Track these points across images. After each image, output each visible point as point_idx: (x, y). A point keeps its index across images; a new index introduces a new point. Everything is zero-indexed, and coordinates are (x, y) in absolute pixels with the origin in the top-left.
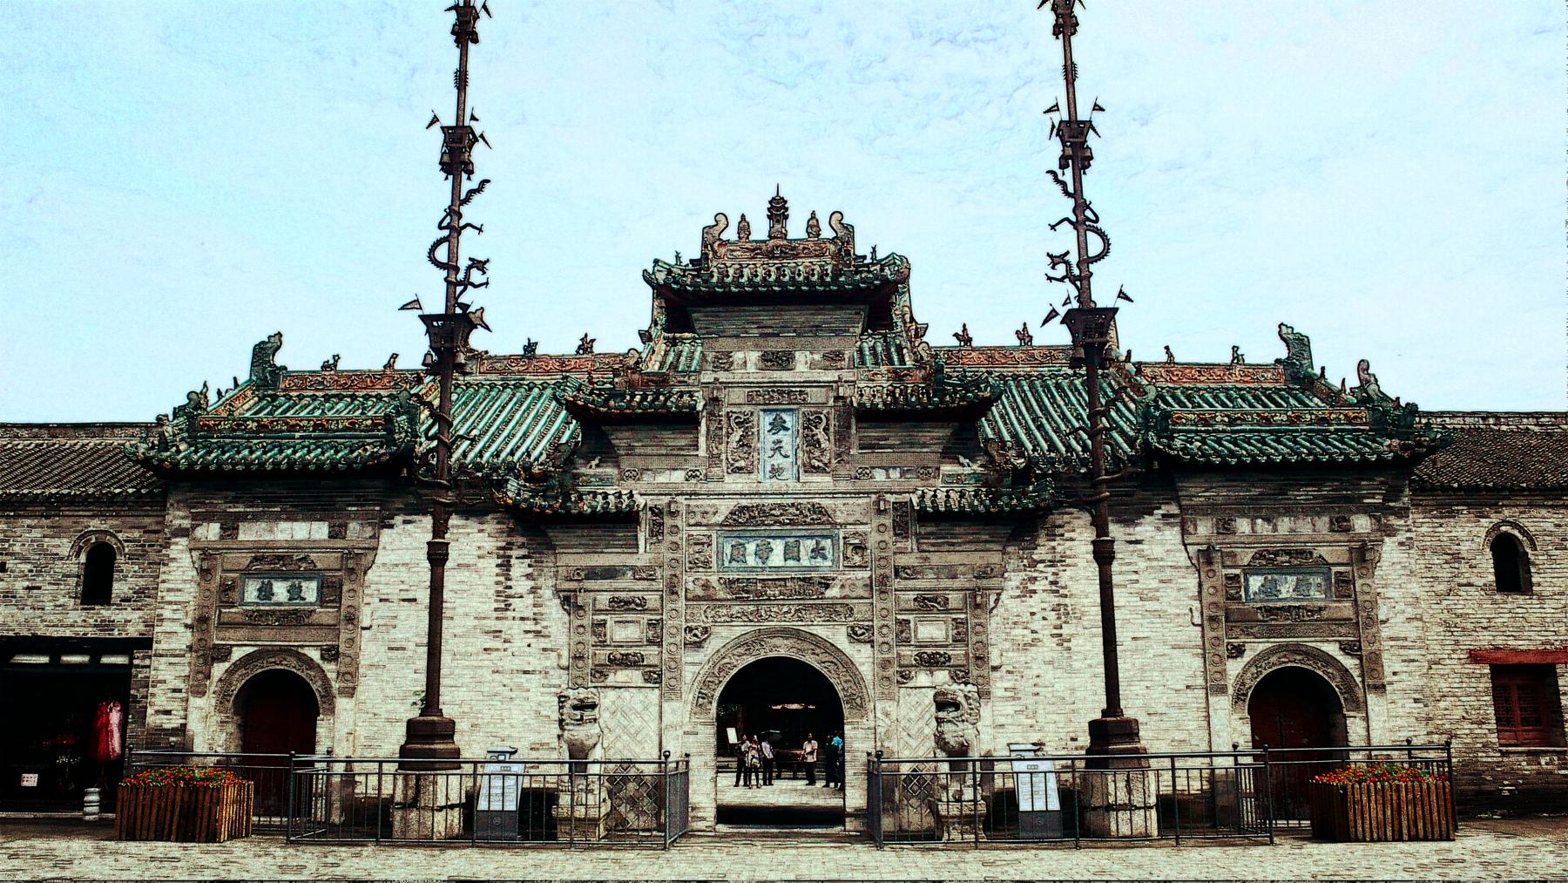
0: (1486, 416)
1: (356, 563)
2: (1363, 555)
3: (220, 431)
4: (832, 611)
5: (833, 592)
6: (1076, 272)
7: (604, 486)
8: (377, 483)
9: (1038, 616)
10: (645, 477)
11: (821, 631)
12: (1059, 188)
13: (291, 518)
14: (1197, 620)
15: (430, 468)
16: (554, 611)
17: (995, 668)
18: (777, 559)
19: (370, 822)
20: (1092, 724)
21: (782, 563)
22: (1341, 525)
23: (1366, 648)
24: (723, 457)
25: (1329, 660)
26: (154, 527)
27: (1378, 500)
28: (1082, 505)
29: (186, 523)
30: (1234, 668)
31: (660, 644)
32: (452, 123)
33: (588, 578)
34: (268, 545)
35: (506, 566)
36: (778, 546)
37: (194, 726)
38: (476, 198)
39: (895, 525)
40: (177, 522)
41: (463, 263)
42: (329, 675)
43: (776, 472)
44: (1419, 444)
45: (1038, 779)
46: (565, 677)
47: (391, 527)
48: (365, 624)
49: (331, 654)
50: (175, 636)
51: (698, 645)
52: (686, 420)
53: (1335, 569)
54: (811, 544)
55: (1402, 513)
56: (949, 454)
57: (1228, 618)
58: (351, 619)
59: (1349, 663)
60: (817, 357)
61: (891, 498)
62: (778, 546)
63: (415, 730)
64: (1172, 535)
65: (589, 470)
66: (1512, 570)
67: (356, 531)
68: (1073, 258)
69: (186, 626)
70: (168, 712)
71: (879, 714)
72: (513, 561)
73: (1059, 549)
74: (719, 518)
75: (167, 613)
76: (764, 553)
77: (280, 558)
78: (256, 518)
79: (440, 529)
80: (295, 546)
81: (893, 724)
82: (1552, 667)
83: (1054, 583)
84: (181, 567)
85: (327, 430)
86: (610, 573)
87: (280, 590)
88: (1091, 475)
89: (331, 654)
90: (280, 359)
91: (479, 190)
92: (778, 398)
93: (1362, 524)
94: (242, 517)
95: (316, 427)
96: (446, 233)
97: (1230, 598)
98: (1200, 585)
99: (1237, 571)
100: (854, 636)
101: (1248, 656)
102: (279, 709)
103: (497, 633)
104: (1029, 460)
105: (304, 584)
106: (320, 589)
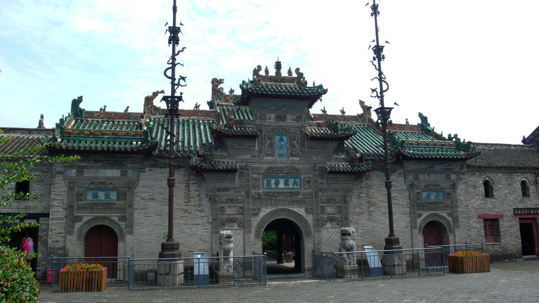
0: (486, 144)
1: (131, 186)
2: (454, 186)
3: (74, 134)
4: (300, 203)
5: (300, 197)
6: (379, 95)
7: (224, 160)
8: (140, 156)
9: (363, 205)
10: (237, 157)
11: (296, 210)
12: (374, 67)
13: (105, 168)
14: (409, 206)
15: (167, 152)
16: (206, 203)
17: (350, 221)
18: (281, 185)
19: (146, 280)
20: (386, 239)
21: (283, 187)
22: (448, 178)
23: (455, 214)
24: (263, 150)
25: (444, 218)
26: (47, 171)
27: (458, 170)
28: (382, 170)
29: (62, 169)
30: (419, 221)
31: (244, 214)
32: (172, 26)
33: (218, 191)
34: (97, 178)
35: (188, 186)
36: (282, 181)
37: (69, 246)
38: (181, 53)
39: (320, 175)
40: (57, 169)
41: (177, 77)
42: (122, 226)
43: (281, 155)
44: (472, 154)
45: (372, 257)
46: (210, 226)
47: (144, 172)
48: (136, 207)
49: (123, 219)
50: (58, 211)
51: (256, 215)
52: (253, 137)
53: (446, 190)
54: (293, 180)
55: (463, 174)
56: (336, 152)
57: (417, 205)
58: (131, 206)
59: (450, 219)
60: (294, 117)
61: (318, 165)
62: (282, 181)
63: (164, 247)
64: (401, 179)
65: (219, 153)
66: (489, 191)
67: (131, 173)
68: (379, 90)
69: (64, 209)
70: (57, 241)
71: (315, 237)
72: (190, 185)
73: (369, 183)
74: (262, 171)
75: (55, 203)
76: (277, 183)
77: (101, 183)
78: (91, 167)
79: (171, 174)
80: (109, 178)
81: (324, 239)
82: (498, 219)
83: (367, 194)
84: (60, 187)
85: (117, 135)
86: (226, 189)
87: (101, 196)
88: (384, 161)
89: (123, 219)
90: (82, 106)
91: (182, 51)
92: (282, 131)
93: (453, 177)
94: (85, 167)
95: (113, 134)
96: (171, 66)
97: (418, 199)
98: (410, 195)
99: (420, 191)
100: (307, 212)
101: (423, 217)
102: (102, 240)
103: (186, 211)
104: (361, 154)
105: (111, 193)
106: (118, 194)
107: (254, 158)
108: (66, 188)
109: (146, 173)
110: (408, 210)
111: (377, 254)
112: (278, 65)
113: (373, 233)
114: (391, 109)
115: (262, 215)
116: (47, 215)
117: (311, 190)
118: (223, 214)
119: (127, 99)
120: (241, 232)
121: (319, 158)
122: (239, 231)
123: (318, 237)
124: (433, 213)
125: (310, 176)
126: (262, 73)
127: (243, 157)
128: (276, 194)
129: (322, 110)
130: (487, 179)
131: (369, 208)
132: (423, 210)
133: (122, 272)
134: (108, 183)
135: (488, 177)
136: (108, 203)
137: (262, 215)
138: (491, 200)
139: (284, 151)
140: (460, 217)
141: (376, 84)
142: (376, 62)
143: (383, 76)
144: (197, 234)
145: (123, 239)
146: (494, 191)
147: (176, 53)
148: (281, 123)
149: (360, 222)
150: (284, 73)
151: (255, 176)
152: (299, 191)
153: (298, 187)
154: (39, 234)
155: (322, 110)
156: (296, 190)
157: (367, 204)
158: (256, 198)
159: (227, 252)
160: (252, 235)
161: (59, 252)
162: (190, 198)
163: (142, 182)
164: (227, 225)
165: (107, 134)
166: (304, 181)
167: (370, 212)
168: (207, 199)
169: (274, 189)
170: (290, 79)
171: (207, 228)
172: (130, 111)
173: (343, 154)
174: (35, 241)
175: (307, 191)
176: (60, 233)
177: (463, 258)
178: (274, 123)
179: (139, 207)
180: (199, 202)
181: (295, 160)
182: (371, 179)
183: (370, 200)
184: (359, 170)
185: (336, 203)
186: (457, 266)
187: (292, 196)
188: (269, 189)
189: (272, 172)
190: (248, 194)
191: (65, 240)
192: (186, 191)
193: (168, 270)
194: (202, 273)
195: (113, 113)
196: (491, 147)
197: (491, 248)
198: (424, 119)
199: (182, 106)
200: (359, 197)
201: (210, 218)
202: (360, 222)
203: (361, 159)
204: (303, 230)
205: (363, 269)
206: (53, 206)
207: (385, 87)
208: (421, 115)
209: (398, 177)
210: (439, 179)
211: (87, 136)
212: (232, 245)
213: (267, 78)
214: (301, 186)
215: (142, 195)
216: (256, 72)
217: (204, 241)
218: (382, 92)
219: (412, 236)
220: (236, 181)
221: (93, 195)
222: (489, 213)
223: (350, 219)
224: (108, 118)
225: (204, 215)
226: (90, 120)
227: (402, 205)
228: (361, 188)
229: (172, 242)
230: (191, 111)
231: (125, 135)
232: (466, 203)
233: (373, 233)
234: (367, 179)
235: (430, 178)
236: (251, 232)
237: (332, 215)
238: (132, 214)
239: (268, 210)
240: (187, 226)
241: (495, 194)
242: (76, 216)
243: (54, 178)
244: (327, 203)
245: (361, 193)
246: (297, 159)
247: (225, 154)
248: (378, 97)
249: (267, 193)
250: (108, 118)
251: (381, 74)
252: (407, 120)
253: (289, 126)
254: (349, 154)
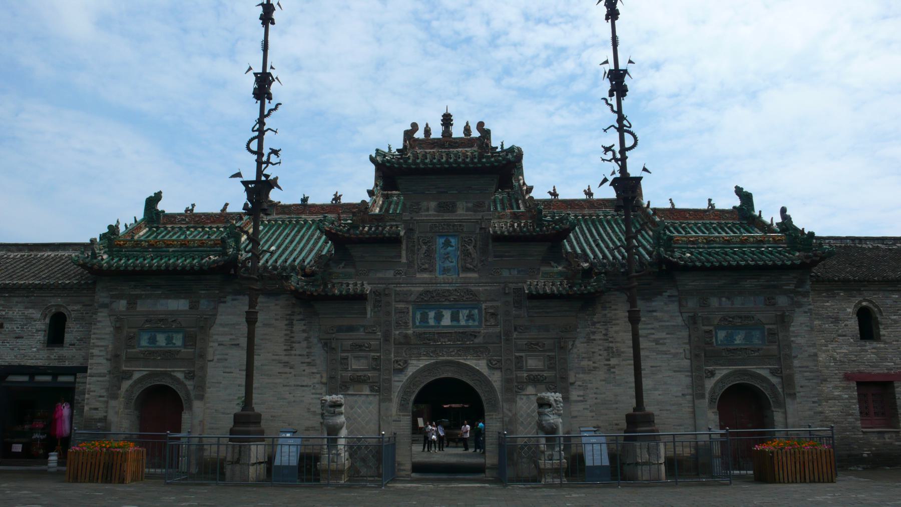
2: (783, 320)
4: (477, 351)
6: (618, 156)
12: (609, 107)
14: (688, 356)
15: (247, 269)
16: (318, 350)
17: (572, 384)
18: (446, 321)
19: (213, 472)
24: (415, 262)
25: (763, 379)
27: (792, 287)
29: (107, 301)
30: (709, 384)
31: (379, 370)
35: (291, 324)
37: (112, 417)
38: (273, 113)
41: (266, 151)
43: (445, 271)
44: (815, 255)
46: (324, 389)
47: (225, 302)
48: (210, 358)
49: (190, 375)
50: (99, 364)
51: (401, 371)
53: (767, 327)
54: (466, 312)
55: (805, 294)
56: (546, 261)
57: (704, 354)
58: (202, 356)
59: (774, 380)
60: (470, 205)
61: (512, 286)
64: (674, 307)
66: (868, 326)
67: (204, 305)
68: (617, 148)
69: (107, 360)
70: (96, 409)
71: (505, 410)
72: (295, 322)
73: (609, 315)
74: (413, 298)
75: (95, 351)
76: (439, 317)
77: (161, 320)
81: (517, 415)
83: (606, 335)
85: (188, 247)
86: (351, 329)
87: (161, 339)
89: (190, 375)
90: (160, 206)
91: (275, 109)
93: (782, 301)
96: (256, 134)
98: (690, 336)
99: (711, 328)
100: (491, 367)
101: (718, 377)
102: (161, 405)
103: (286, 364)
104: (591, 264)
105: (174, 335)
106: (184, 338)
107: (398, 276)
108: (112, 329)
110: (686, 363)
111: (603, 440)
112: (447, 120)
113: (615, 406)
114: (640, 178)
115: (411, 371)
116: (84, 369)
117: (498, 329)
118: (346, 370)
119: (217, 192)
120: (374, 400)
121: (515, 273)
122: (371, 398)
123: (510, 411)
124: (740, 370)
125: (498, 304)
126: (420, 135)
127: (380, 275)
128: (436, 336)
129: (550, 192)
130: (864, 304)
131: (609, 360)
132: (717, 364)
133: (185, 459)
134: (170, 320)
135: (865, 300)
136: (170, 352)
137: (411, 371)
138: (875, 344)
139: (452, 264)
140: (797, 377)
141: (613, 139)
142: (613, 101)
143: (625, 122)
144: (302, 401)
145: (190, 408)
146: (881, 327)
147: (266, 113)
148: (447, 217)
149: (590, 385)
150: (457, 132)
151: (401, 306)
152: (478, 330)
153: (476, 323)
154: (76, 397)
155: (550, 192)
156: (472, 329)
157: (605, 353)
158: (400, 343)
159: (333, 431)
160: (394, 407)
161: (99, 424)
162: (293, 342)
163: (221, 318)
164: (351, 388)
165: (173, 246)
166: (486, 313)
167: (610, 368)
168: (320, 345)
169: (432, 327)
170: (467, 141)
171: (319, 391)
172: (229, 210)
173: (559, 264)
174: (72, 408)
175: (491, 330)
176: (100, 396)
177: (772, 453)
178: (434, 216)
179: (216, 358)
180: (307, 350)
181: (470, 278)
182: (613, 307)
183: (611, 345)
184: (586, 292)
186: (765, 472)
187: (464, 340)
189: (431, 300)
190: (387, 337)
191: (107, 407)
192: (288, 332)
193: (236, 456)
194: (285, 462)
195: (204, 214)
196: (894, 244)
197: (874, 439)
198: (746, 197)
199: (274, 195)
200: (589, 341)
201: (325, 375)
202: (590, 385)
203: (587, 273)
204: (483, 399)
205: (576, 470)
206: (93, 356)
207: (629, 141)
208: (739, 191)
209: (666, 304)
211: (145, 249)
212: (342, 419)
213: (427, 141)
214: (480, 322)
215: (221, 339)
216: (408, 135)
217: (314, 413)
218: (623, 150)
219: (694, 412)
220: (369, 316)
221: (149, 339)
222: (870, 370)
223: (572, 380)
224: (196, 222)
225: (315, 371)
226: (169, 226)
227: (675, 355)
228: (594, 324)
229: (250, 413)
230: (327, 206)
231: (199, 246)
232: (812, 350)
233: (615, 406)
234: (604, 308)
235: (733, 304)
236: (390, 400)
237: (536, 373)
238: (203, 368)
239: (422, 364)
240: (287, 388)
241: (882, 332)
242: (124, 372)
243: (95, 313)
245: (594, 333)
246: (475, 275)
247: (350, 270)
248: (616, 160)
249: (420, 334)
250: (196, 222)
251: (621, 118)
252: (710, 200)
253: (460, 221)
254: (570, 265)
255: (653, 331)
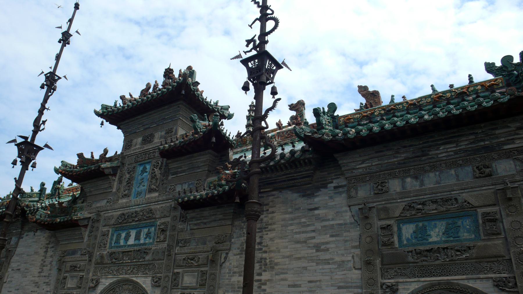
11: (140, 280)
22: (484, 173)
43: (139, 194)
53: (480, 211)
74: (112, 222)
99: (388, 222)
109: (24, 239)
110: (355, 275)
124: (439, 283)
153: (151, 241)
163: (19, 250)
181: (152, 198)
182: (271, 210)
183: (264, 255)
185: (199, 266)
188: (117, 247)
189: (125, 222)
210: (453, 181)
214: (154, 239)
227: (341, 265)
244: (186, 267)
246: (156, 194)
255: (313, 234)
